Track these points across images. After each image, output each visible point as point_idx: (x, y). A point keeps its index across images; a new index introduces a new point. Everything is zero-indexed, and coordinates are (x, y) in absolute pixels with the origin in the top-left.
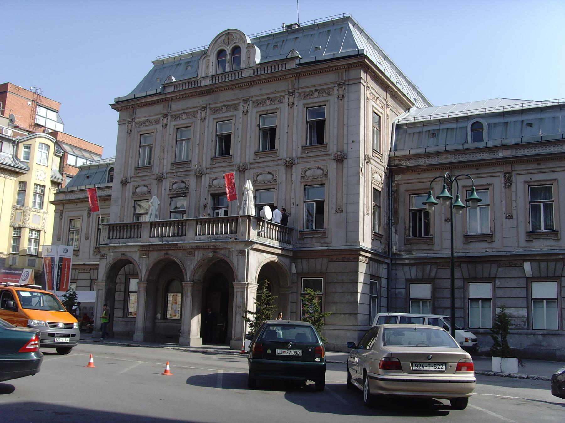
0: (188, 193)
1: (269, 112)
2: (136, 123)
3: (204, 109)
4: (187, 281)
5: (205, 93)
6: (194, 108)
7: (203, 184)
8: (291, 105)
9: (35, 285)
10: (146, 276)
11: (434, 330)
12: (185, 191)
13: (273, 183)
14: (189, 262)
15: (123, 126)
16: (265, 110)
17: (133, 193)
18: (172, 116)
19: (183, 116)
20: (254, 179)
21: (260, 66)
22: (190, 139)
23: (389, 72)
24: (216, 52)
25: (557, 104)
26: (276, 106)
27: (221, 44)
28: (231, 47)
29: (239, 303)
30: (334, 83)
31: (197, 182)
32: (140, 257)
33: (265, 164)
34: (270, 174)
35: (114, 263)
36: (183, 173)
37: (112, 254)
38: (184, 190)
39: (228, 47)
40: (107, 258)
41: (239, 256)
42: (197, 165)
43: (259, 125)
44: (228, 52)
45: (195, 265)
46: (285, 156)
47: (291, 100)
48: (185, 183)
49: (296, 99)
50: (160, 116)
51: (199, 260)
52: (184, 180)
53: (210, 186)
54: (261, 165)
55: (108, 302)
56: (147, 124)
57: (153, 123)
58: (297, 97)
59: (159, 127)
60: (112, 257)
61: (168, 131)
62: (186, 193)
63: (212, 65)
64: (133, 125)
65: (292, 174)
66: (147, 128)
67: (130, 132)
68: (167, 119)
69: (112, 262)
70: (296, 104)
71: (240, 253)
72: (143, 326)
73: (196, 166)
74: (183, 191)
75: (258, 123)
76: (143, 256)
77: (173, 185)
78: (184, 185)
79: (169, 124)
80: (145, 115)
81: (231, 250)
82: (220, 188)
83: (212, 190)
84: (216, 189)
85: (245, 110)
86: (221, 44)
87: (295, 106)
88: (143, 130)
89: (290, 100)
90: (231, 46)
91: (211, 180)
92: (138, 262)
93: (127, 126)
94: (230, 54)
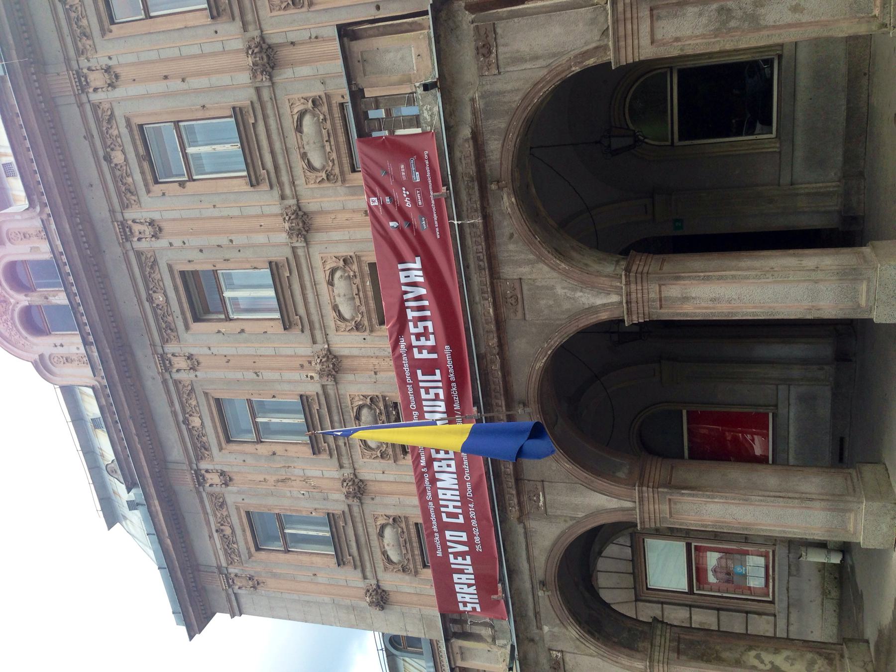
0: (384, 398)
1: (142, 151)
2: (231, 563)
3: (166, 363)
4: (621, 303)
5: (125, 360)
6: (168, 392)
7: (355, 352)
8: (113, 78)
9: (768, 429)
10: (615, 489)
11: (731, 535)
12: (382, 408)
13: (325, 109)
14: (543, 302)
15: (243, 600)
16: (141, 167)
17: (404, 571)
18: (199, 458)
19: (193, 424)
20: (322, 180)
21: (35, 197)
22: (249, 401)
23: (667, 600)
24: (30, 338)
25: (567, 338)
26: (124, 131)
27: (9, 323)
28: (12, 292)
29: (704, 20)
30: (81, 105)
31: (353, 370)
32: (546, 515)
33: (278, 146)
34: (301, 125)
35: (580, 623)
36: (336, 418)
37: (546, 629)
38: (378, 411)
39: (12, 301)
40: (562, 652)
41: (501, 57)
42: (309, 375)
43: (182, 184)
44: (22, 300)
45: (555, 274)
46: (244, 77)
47: (97, 79)
48: (360, 408)
49: (93, 64)
50: (204, 495)
51: (532, 257)
52: (353, 415)
53: (358, 327)
54: (281, 161)
55: (725, 655)
56: (228, 531)
57: (225, 514)
58: (89, 61)
59: (232, 496)
60: (556, 630)
61: (235, 469)
62: (386, 406)
63: (62, 345)
64: (236, 571)
65: (293, 43)
66: (239, 532)
67: (255, 584)
68: (207, 471)
69: (573, 632)
70: (104, 62)
71: (490, 52)
72: (823, 504)
73: (312, 377)
74: (381, 413)
75: (177, 184)
76: (541, 503)
77: (369, 447)
78: (365, 412)
79: (219, 467)
80: (208, 538)
81: (480, 104)
82: (361, 294)
83: (370, 320)
84: (363, 309)
85: (148, 231)
86: (9, 323)
87: (110, 63)
88: (244, 540)
89: (98, 84)
90: (9, 294)
91: (342, 325)
92: (563, 526)
93: (240, 591)
94: (26, 296)
